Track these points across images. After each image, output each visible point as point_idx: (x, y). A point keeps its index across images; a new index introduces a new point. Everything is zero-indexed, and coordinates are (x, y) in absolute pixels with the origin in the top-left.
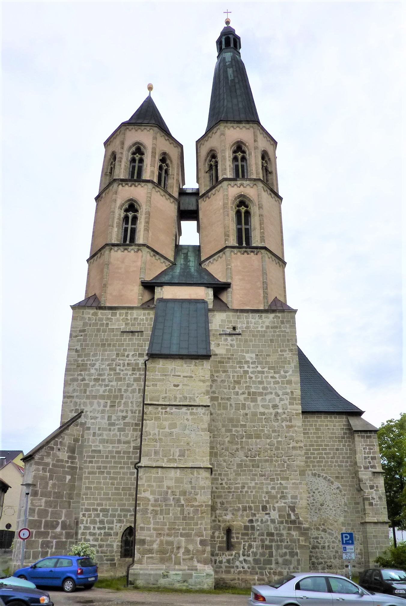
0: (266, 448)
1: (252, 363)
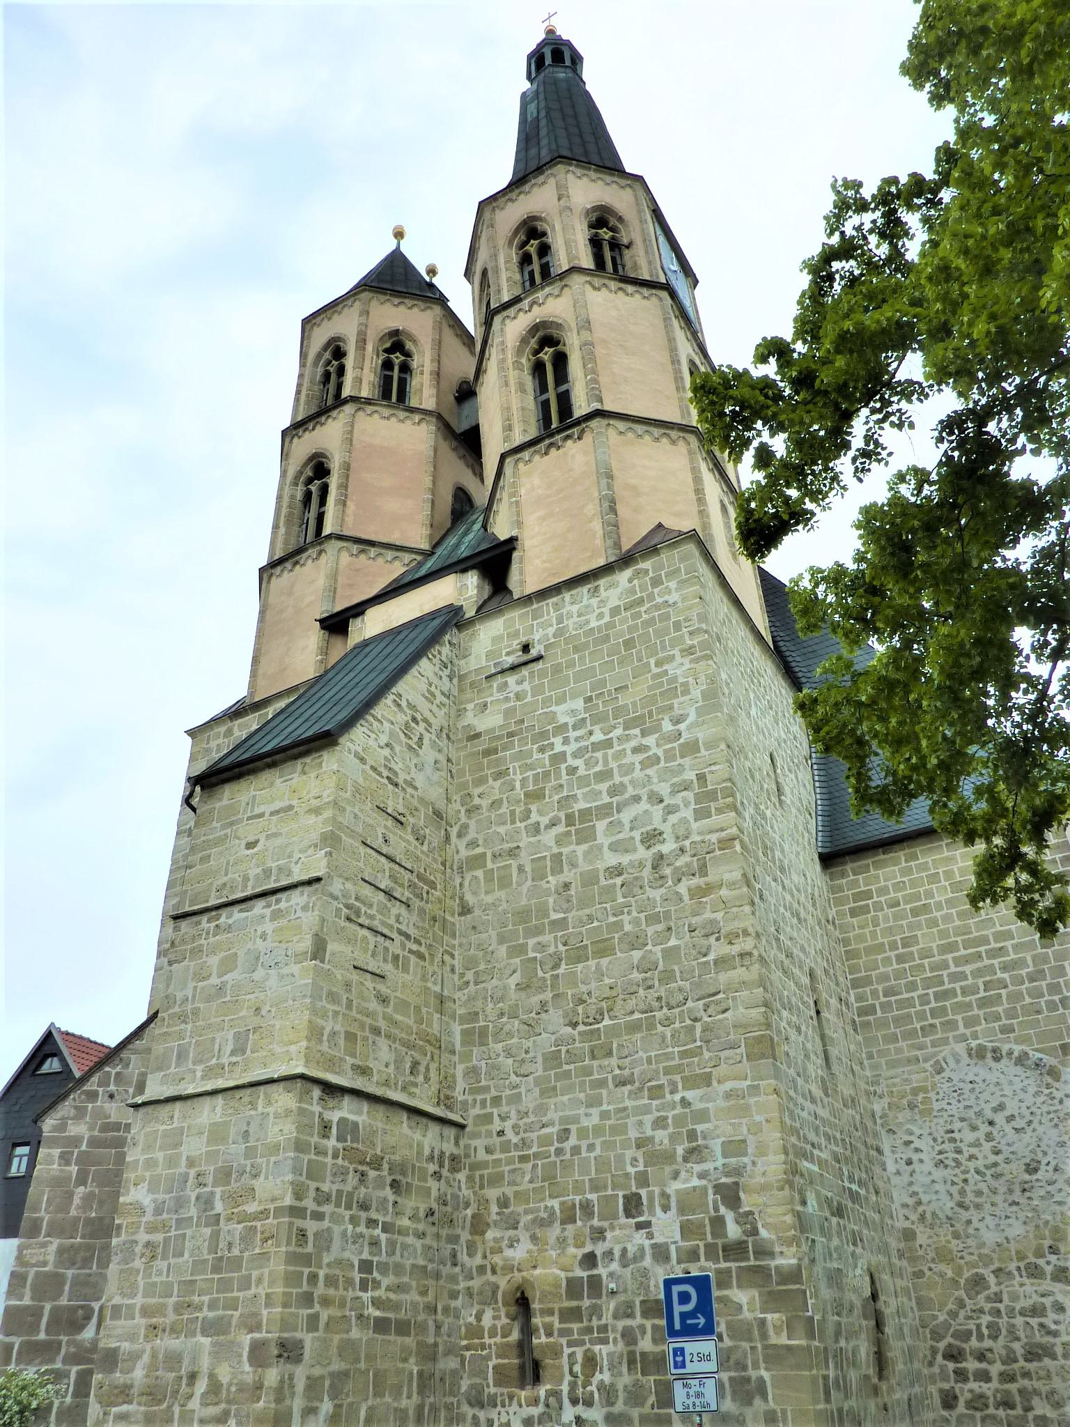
0: (630, 983)
1: (575, 727)
